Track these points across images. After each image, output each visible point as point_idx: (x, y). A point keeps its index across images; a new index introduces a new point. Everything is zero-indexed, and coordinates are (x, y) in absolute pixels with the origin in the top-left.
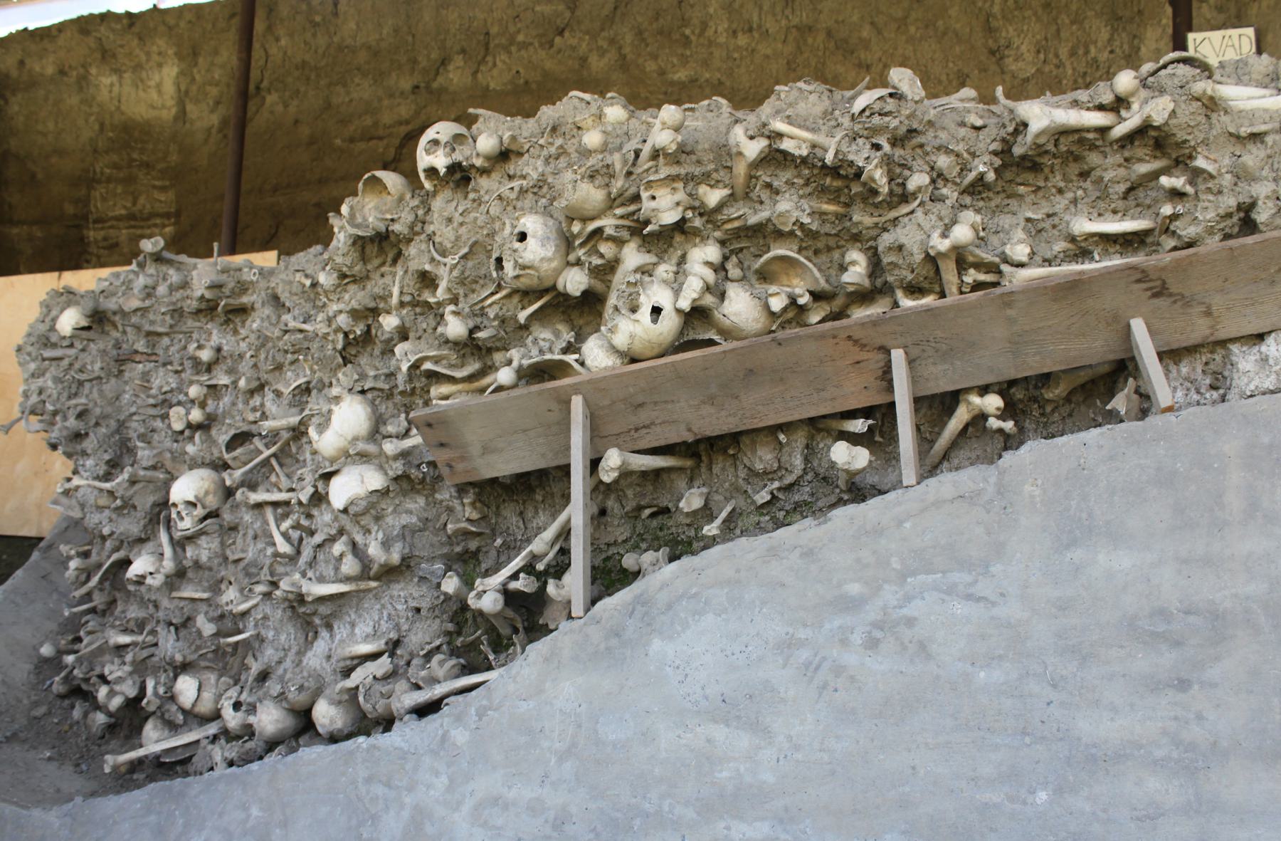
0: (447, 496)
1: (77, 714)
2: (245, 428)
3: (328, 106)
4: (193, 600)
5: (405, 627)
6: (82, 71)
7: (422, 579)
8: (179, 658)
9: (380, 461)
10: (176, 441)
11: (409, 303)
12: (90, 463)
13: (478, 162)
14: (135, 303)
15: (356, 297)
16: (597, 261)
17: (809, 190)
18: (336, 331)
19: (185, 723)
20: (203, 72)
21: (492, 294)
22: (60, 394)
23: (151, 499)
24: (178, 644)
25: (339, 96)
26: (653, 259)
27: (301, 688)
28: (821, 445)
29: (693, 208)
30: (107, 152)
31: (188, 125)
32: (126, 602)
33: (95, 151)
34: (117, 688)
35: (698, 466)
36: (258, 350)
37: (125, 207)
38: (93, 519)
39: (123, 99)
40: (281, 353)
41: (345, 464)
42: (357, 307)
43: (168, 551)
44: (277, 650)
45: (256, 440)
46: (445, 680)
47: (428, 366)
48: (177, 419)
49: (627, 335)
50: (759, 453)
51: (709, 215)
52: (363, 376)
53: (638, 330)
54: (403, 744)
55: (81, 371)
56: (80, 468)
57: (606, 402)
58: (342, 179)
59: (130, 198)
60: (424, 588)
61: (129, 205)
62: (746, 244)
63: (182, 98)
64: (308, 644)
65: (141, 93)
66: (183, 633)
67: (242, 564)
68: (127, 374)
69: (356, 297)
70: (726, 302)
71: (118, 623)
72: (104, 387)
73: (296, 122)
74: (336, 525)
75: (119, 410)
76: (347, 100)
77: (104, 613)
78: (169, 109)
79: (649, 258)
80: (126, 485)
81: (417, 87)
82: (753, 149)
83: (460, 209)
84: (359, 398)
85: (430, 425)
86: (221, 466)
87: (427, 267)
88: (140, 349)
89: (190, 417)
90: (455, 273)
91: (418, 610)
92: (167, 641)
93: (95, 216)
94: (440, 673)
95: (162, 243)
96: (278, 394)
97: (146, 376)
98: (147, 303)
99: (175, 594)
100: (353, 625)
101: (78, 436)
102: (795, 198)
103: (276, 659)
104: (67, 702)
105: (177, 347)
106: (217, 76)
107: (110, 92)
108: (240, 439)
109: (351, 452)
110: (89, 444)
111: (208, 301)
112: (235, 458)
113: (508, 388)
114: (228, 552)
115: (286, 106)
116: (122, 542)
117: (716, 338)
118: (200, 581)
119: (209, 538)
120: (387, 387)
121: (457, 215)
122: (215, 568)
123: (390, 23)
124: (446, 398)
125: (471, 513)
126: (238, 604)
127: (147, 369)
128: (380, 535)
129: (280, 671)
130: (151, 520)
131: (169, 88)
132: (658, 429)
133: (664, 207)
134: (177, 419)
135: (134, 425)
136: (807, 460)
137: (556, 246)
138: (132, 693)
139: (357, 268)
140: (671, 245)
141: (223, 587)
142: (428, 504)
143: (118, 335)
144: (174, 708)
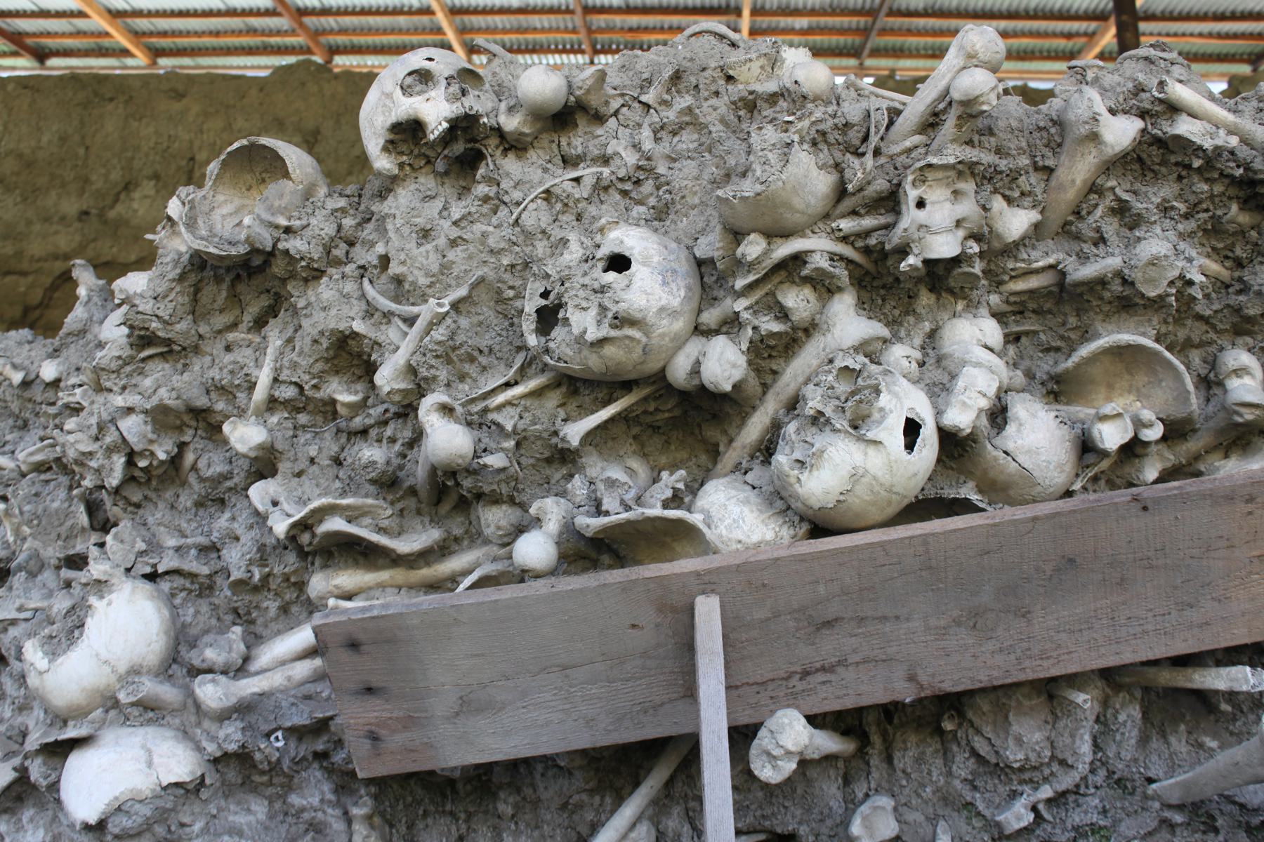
0: (315, 801)
9: (186, 718)
11: (286, 403)
13: (511, 123)
15: (164, 384)
16: (771, 325)
17: (1191, 225)
18: (110, 451)
21: (508, 385)
26: (884, 332)
28: (1122, 717)
29: (976, 237)
35: (861, 753)
41: (103, 723)
42: (170, 402)
49: (845, 471)
50: (1015, 728)
51: (996, 252)
52: (153, 547)
53: (874, 462)
57: (760, 614)
62: (1052, 318)
69: (164, 384)
70: (1010, 429)
79: (876, 329)
81: (86, 213)
82: (1121, 132)
83: (457, 211)
84: (148, 586)
85: (354, 645)
87: (358, 326)
90: (439, 334)
102: (1171, 234)
109: (122, 697)
113: (538, 576)
117: (974, 497)
120: (205, 570)
121: (446, 224)
123: (55, 128)
124: (349, 597)
132: (848, 674)
133: (937, 224)
136: (1096, 746)
137: (689, 288)
139: (181, 327)
140: (909, 311)
142: (271, 817)
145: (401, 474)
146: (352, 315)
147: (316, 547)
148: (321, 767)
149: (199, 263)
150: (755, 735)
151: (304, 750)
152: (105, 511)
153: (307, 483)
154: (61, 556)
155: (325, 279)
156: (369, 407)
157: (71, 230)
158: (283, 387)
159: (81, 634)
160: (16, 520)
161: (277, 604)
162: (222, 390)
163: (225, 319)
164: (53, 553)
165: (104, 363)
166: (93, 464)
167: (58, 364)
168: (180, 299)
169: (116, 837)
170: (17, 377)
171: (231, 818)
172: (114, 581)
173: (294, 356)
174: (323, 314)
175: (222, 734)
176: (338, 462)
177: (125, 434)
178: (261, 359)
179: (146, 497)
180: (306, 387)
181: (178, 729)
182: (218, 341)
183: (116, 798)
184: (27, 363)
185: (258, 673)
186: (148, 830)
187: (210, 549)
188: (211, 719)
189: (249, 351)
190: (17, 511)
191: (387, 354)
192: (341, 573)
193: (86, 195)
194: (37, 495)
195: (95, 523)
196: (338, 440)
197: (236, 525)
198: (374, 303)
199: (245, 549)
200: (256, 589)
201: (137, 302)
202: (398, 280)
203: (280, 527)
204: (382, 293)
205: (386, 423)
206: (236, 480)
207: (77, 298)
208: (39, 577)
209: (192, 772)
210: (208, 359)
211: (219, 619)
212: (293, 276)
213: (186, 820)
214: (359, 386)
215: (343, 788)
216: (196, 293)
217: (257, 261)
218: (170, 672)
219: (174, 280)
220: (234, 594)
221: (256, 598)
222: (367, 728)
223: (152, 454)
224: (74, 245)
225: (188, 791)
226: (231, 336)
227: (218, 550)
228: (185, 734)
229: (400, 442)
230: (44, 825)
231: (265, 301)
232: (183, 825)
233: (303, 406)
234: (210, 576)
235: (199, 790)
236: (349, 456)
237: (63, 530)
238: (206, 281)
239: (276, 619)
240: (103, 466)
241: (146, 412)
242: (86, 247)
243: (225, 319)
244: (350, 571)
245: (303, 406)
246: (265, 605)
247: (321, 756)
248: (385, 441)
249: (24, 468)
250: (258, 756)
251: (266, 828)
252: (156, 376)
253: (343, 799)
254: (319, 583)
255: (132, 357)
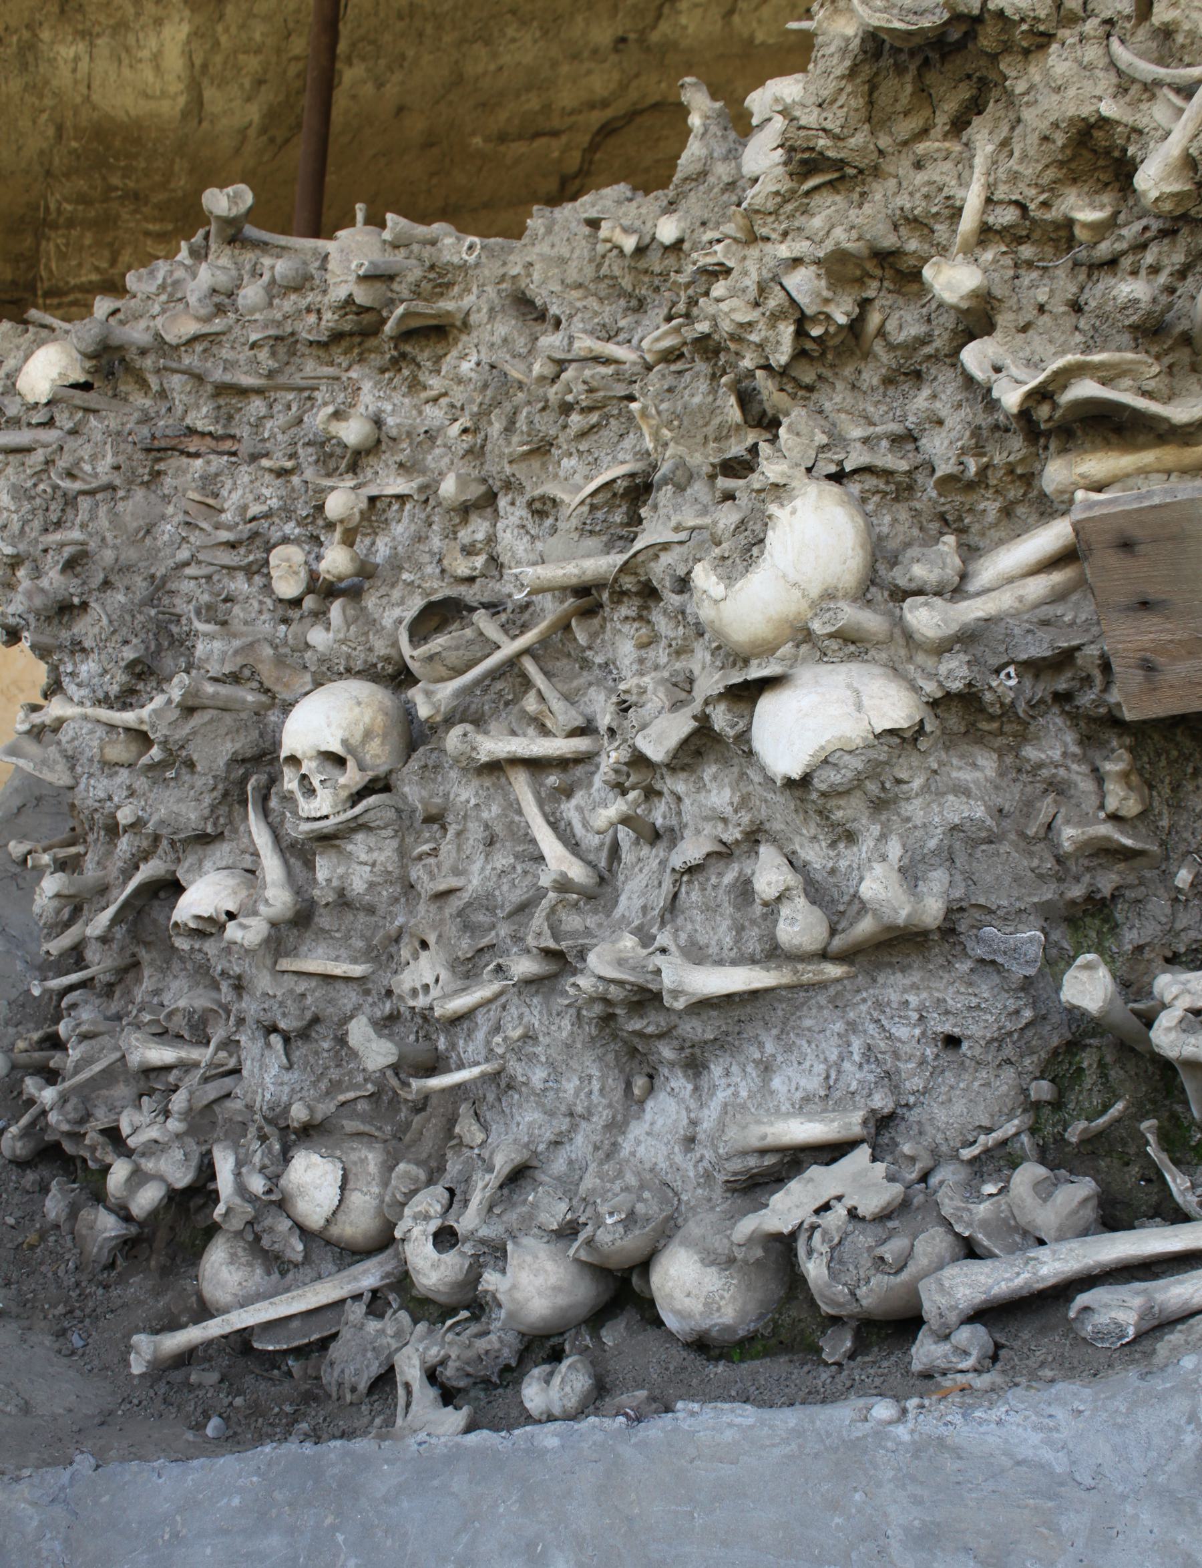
0: (1056, 754)
1: (54, 1205)
2: (443, 591)
3: (458, 79)
4: (328, 978)
5: (917, 1083)
6: (26, 35)
7: (986, 964)
8: (298, 1113)
10: (285, 621)
12: (88, 668)
14: (191, 328)
15: (836, 222)
18: (775, 318)
19: (307, 1258)
20: (233, 30)
22: (25, 523)
23: (227, 748)
24: (286, 1077)
25: (478, 62)
27: (630, 1220)
30: (67, 175)
31: (205, 124)
32: (164, 971)
33: (48, 173)
34: (148, 1165)
36: (484, 414)
37: (97, 269)
38: (93, 789)
39: (96, 84)
40: (550, 416)
42: (850, 246)
43: (272, 866)
44: (551, 1114)
45: (481, 618)
46: (1060, 1238)
47: (1086, 389)
48: (287, 574)
52: (836, 440)
54: (1046, 1454)
55: (71, 475)
56: (66, 680)
58: (486, 206)
59: (106, 253)
60: (985, 990)
61: (104, 265)
63: (197, 78)
64: (633, 1104)
65: (126, 72)
66: (301, 1050)
67: (455, 903)
68: (168, 481)
69: (836, 222)
71: (147, 1017)
72: (121, 506)
73: (400, 110)
74: (746, 818)
75: (153, 555)
76: (492, 67)
77: (109, 990)
78: (174, 98)
80: (175, 714)
81: (623, 40)
84: (834, 488)
85: (1126, 545)
86: (400, 678)
87: (1108, 108)
88: (200, 425)
89: (323, 566)
91: (952, 1042)
92: (263, 1067)
93: (46, 285)
94: (1045, 1217)
95: (248, 198)
96: (543, 508)
97: (209, 483)
98: (218, 324)
99: (285, 964)
100: (767, 1068)
101: (65, 610)
103: (549, 1135)
104: (31, 1177)
105: (281, 419)
106: (257, 36)
107: (74, 70)
108: (439, 615)
109: (816, 626)
110: (86, 628)
111: (363, 310)
112: (431, 658)
114: (416, 872)
115: (380, 85)
116: (156, 839)
118: (347, 937)
119: (372, 840)
120: (903, 466)
122: (382, 909)
125: (1118, 797)
126: (446, 996)
127: (213, 469)
128: (894, 849)
129: (559, 1165)
130: (226, 794)
131: (174, 62)
134: (287, 574)
135: (187, 586)
138: (182, 1178)
141: (405, 953)
142: (1002, 774)
143: (148, 402)
144: (284, 1225)
145: (1169, 317)
146: (1098, 93)
147: (1058, 423)
148: (1063, 712)
149: (875, 45)
150: (213, 1317)
151: (1042, 690)
152: (761, 402)
153: (1037, 338)
154: (716, 461)
155: (1054, 47)
156: (1120, 227)
157: (607, 65)
158: (999, 210)
159: (762, 553)
160: (653, 422)
161: (998, 505)
162: (916, 223)
163: (912, 124)
164: (702, 459)
165: (758, 201)
166: (754, 338)
167: (679, 220)
168: (853, 103)
169: (824, 794)
170: (629, 244)
171: (954, 774)
172: (794, 484)
173: (1013, 163)
174: (1056, 98)
175: (943, 669)
176: (1076, 307)
177: (794, 294)
178: (966, 174)
179: (820, 377)
180: (1032, 206)
181: (886, 666)
182: (903, 156)
183: (823, 748)
184: (638, 223)
185: (978, 594)
186: (858, 787)
187: (906, 439)
188: (927, 652)
189: (948, 166)
190: (653, 411)
191: (1152, 144)
192: (1087, 457)
193: (620, 15)
194: (670, 390)
195: (749, 418)
196: (1075, 277)
197: (938, 405)
198: (1129, 71)
199: (954, 434)
200: (971, 486)
201: (797, 113)
202: (1167, 33)
203: (1011, 398)
204: (1141, 55)
205: (1144, 246)
206: (938, 343)
207: (688, 131)
208: (689, 491)
209: (910, 717)
210: (892, 182)
211: (921, 529)
212: (1007, 48)
213: (903, 775)
214: (1106, 198)
215: (1089, 738)
216: (871, 93)
217: (955, 35)
218: (869, 596)
219: (842, 77)
220: (940, 495)
221: (968, 499)
222: (1139, 655)
223: (828, 317)
224: (613, 86)
225: (904, 739)
226: (921, 148)
227: (916, 440)
228: (895, 670)
229: (1166, 272)
230: (730, 784)
231: (965, 92)
232: (899, 782)
233: (1030, 235)
234: (909, 473)
235: (916, 740)
236: (1092, 298)
237: (710, 430)
238: (884, 73)
239: (995, 525)
240: (766, 339)
241: (818, 262)
242: (627, 86)
243: (912, 124)
244: (1099, 455)
245: (1030, 235)
246: (981, 507)
247: (1063, 698)
248: (1143, 272)
249: (649, 358)
250: (988, 697)
251: (997, 788)
252: (824, 214)
253: (1090, 753)
254: (1057, 473)
255: (793, 192)
